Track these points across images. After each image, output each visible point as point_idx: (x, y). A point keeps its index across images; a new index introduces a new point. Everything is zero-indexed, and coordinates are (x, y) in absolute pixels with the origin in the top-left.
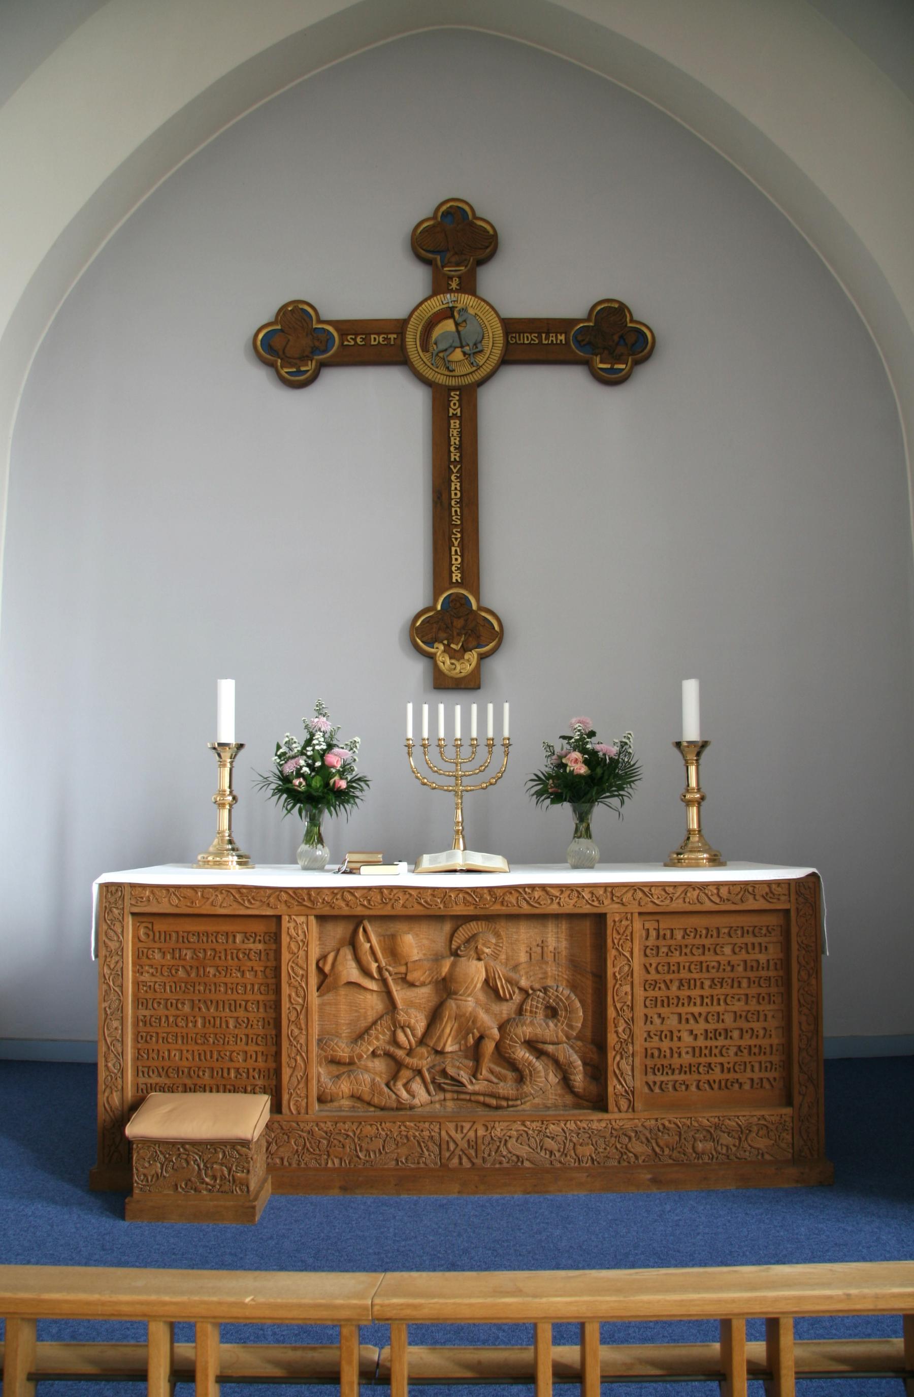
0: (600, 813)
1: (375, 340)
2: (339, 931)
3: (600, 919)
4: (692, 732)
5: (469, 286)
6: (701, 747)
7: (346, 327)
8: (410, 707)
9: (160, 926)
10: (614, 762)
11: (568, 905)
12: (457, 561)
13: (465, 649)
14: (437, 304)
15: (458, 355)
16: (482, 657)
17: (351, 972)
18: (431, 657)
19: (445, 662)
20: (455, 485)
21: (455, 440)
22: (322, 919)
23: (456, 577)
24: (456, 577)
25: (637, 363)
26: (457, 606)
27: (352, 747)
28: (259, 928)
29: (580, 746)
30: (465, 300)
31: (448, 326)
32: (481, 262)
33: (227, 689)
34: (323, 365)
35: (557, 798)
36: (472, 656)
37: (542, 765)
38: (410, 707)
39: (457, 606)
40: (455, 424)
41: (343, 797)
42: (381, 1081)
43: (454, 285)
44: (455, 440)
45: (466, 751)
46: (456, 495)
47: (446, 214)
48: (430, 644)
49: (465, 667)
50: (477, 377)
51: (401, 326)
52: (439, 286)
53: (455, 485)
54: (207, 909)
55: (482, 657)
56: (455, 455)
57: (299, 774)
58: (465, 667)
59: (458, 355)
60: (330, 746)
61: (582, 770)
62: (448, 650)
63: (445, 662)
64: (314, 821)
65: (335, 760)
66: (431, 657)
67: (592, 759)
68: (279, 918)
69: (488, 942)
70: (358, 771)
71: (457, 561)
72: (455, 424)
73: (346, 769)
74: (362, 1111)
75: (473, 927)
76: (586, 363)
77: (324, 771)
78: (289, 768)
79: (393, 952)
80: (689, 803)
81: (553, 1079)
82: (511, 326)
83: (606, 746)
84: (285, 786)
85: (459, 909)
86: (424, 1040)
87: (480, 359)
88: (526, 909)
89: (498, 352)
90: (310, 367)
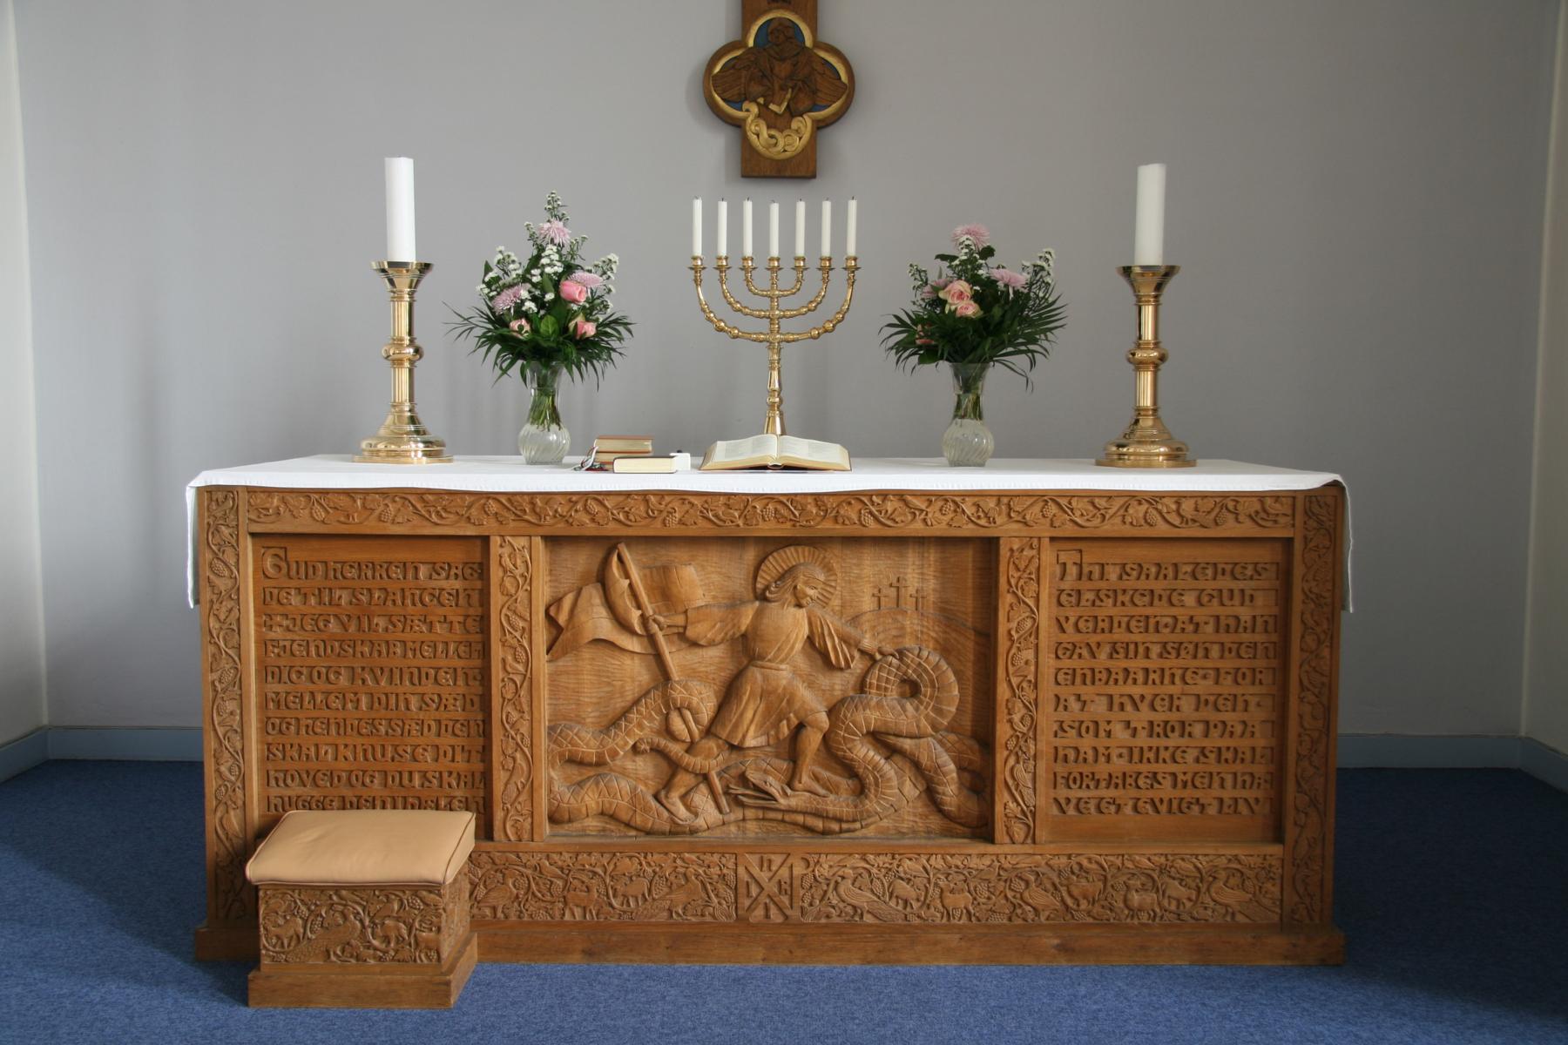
0: (998, 379)
2: (581, 561)
3: (989, 545)
4: (1149, 250)
8: (698, 205)
9: (297, 553)
10: (1022, 299)
13: (792, 113)
16: (820, 126)
17: (598, 623)
18: (738, 125)
19: (759, 134)
22: (552, 541)
26: (780, 40)
27: (605, 269)
28: (455, 555)
29: (967, 269)
33: (402, 173)
36: (804, 124)
37: (908, 302)
38: (698, 205)
39: (780, 40)
41: (590, 349)
45: (787, 279)
48: (737, 103)
49: (791, 142)
54: (371, 527)
57: (520, 313)
58: (791, 142)
60: (569, 269)
61: (970, 309)
62: (764, 113)
63: (759, 134)
65: (576, 290)
66: (738, 125)
67: (987, 293)
68: (485, 540)
69: (813, 577)
70: (614, 308)
74: (617, 836)
75: (791, 555)
78: (504, 303)
79: (665, 594)
80: (1139, 366)
81: (911, 790)
83: (1010, 272)
84: (499, 333)
85: (768, 528)
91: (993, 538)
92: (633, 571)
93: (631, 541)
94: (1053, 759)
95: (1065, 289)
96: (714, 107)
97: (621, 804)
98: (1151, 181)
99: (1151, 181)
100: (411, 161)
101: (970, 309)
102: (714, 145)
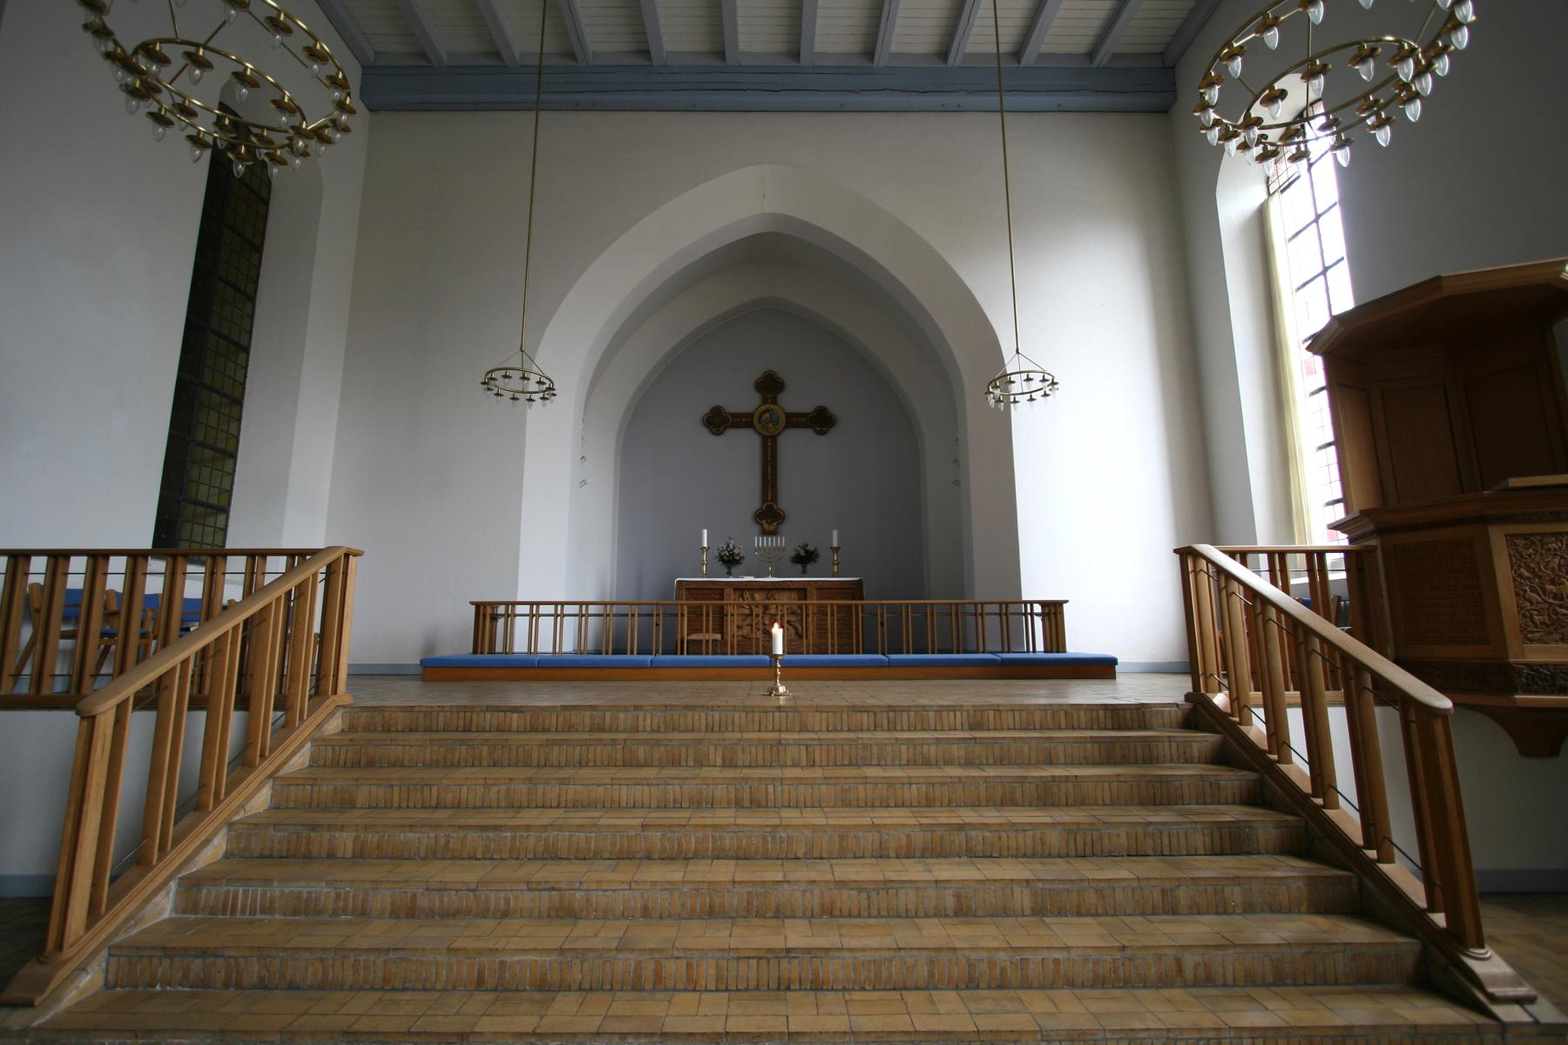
0: (809, 567)
1: (743, 420)
2: (739, 593)
3: (805, 589)
4: (835, 544)
5: (774, 402)
6: (838, 549)
7: (734, 415)
8: (756, 538)
9: (693, 592)
10: (813, 553)
11: (797, 586)
12: (770, 493)
13: (773, 522)
14: (764, 407)
15: (770, 425)
16: (778, 524)
18: (762, 524)
19: (766, 526)
20: (769, 469)
21: (769, 454)
22: (735, 589)
23: (770, 498)
24: (770, 498)
25: (830, 427)
26: (770, 508)
27: (740, 548)
28: (718, 592)
29: (803, 548)
30: (773, 406)
31: (768, 415)
32: (778, 392)
33: (705, 531)
34: (726, 428)
35: (797, 563)
36: (775, 524)
37: (793, 554)
38: (756, 538)
39: (770, 508)
40: (769, 449)
41: (737, 562)
42: (749, 632)
43: (769, 401)
44: (769, 454)
45: (772, 551)
46: (770, 472)
47: (767, 376)
50: (778, 432)
51: (751, 415)
52: (765, 401)
53: (769, 469)
54: (705, 587)
55: (778, 524)
56: (769, 459)
57: (726, 555)
58: (772, 527)
59: (770, 425)
60: (734, 548)
61: (803, 554)
62: (767, 523)
63: (766, 526)
64: (729, 568)
65: (736, 551)
66: (762, 524)
67: (807, 552)
68: (723, 589)
70: (742, 555)
71: (770, 493)
72: (769, 449)
73: (738, 555)
74: (744, 639)
75: (773, 592)
76: (813, 427)
77: (733, 554)
78: (723, 554)
80: (834, 564)
81: (793, 631)
82: (788, 415)
83: (811, 548)
84: (722, 558)
85: (769, 587)
86: (740, 960)
87: (778, 427)
88: (786, 587)
89: (783, 425)
90: (722, 428)
91: (1248, 913)
92: (747, 595)
93: (748, 589)
94: (226, 25)
95: (821, 552)
96: (757, 521)
97: (745, 635)
98: (835, 533)
99: (835, 533)
100: (200, 597)
101: (803, 554)
102: (756, 528)
